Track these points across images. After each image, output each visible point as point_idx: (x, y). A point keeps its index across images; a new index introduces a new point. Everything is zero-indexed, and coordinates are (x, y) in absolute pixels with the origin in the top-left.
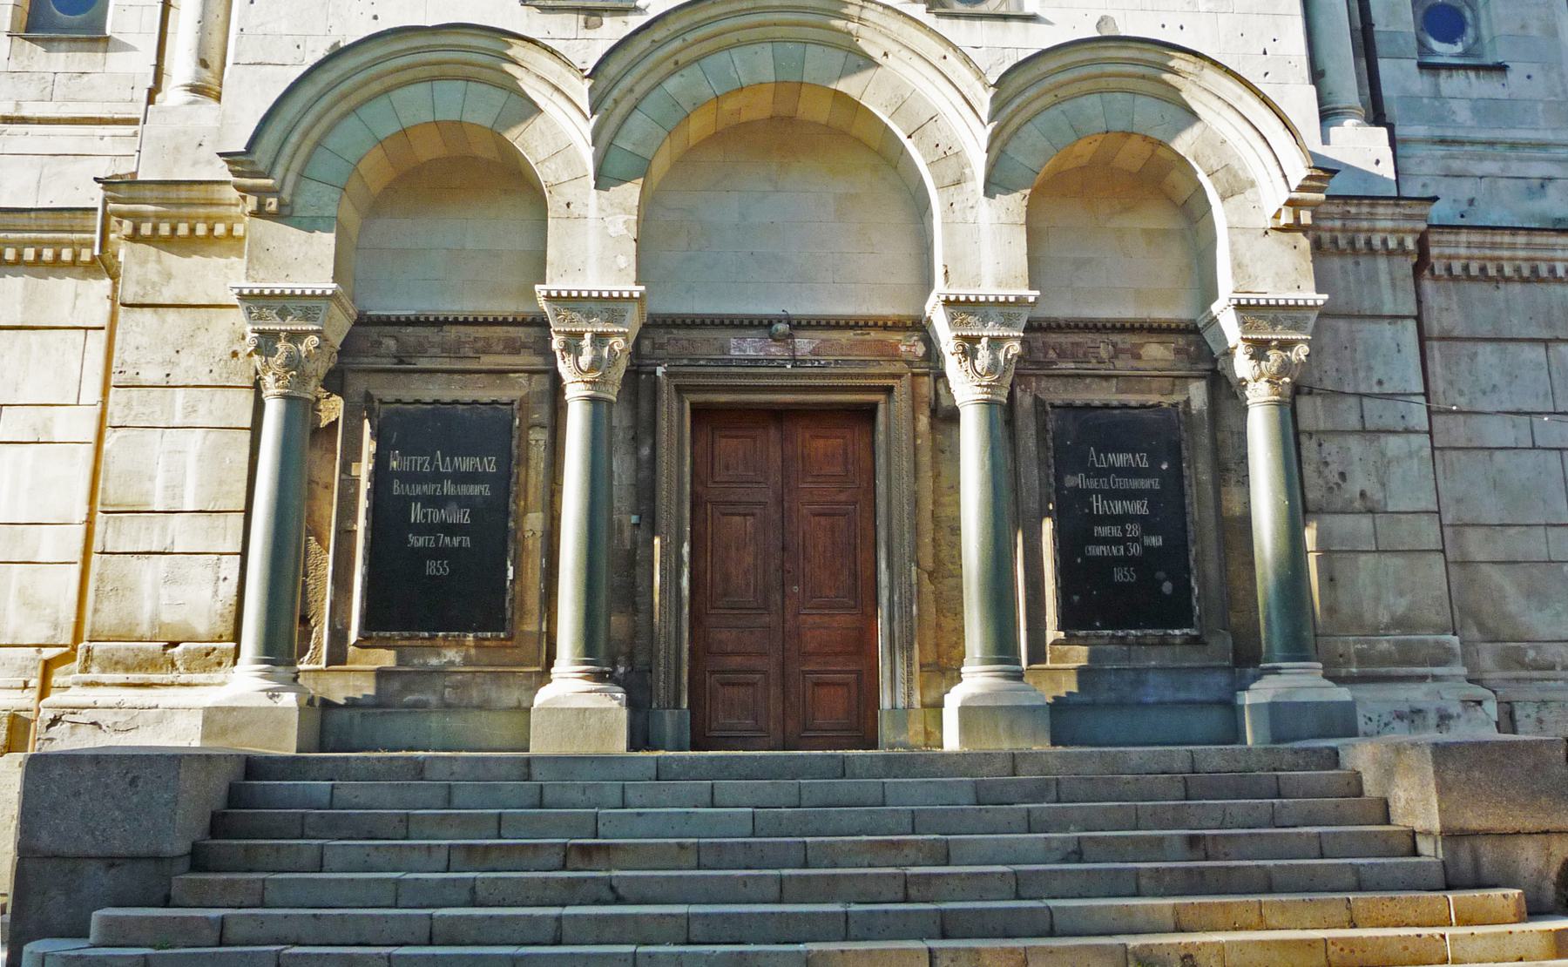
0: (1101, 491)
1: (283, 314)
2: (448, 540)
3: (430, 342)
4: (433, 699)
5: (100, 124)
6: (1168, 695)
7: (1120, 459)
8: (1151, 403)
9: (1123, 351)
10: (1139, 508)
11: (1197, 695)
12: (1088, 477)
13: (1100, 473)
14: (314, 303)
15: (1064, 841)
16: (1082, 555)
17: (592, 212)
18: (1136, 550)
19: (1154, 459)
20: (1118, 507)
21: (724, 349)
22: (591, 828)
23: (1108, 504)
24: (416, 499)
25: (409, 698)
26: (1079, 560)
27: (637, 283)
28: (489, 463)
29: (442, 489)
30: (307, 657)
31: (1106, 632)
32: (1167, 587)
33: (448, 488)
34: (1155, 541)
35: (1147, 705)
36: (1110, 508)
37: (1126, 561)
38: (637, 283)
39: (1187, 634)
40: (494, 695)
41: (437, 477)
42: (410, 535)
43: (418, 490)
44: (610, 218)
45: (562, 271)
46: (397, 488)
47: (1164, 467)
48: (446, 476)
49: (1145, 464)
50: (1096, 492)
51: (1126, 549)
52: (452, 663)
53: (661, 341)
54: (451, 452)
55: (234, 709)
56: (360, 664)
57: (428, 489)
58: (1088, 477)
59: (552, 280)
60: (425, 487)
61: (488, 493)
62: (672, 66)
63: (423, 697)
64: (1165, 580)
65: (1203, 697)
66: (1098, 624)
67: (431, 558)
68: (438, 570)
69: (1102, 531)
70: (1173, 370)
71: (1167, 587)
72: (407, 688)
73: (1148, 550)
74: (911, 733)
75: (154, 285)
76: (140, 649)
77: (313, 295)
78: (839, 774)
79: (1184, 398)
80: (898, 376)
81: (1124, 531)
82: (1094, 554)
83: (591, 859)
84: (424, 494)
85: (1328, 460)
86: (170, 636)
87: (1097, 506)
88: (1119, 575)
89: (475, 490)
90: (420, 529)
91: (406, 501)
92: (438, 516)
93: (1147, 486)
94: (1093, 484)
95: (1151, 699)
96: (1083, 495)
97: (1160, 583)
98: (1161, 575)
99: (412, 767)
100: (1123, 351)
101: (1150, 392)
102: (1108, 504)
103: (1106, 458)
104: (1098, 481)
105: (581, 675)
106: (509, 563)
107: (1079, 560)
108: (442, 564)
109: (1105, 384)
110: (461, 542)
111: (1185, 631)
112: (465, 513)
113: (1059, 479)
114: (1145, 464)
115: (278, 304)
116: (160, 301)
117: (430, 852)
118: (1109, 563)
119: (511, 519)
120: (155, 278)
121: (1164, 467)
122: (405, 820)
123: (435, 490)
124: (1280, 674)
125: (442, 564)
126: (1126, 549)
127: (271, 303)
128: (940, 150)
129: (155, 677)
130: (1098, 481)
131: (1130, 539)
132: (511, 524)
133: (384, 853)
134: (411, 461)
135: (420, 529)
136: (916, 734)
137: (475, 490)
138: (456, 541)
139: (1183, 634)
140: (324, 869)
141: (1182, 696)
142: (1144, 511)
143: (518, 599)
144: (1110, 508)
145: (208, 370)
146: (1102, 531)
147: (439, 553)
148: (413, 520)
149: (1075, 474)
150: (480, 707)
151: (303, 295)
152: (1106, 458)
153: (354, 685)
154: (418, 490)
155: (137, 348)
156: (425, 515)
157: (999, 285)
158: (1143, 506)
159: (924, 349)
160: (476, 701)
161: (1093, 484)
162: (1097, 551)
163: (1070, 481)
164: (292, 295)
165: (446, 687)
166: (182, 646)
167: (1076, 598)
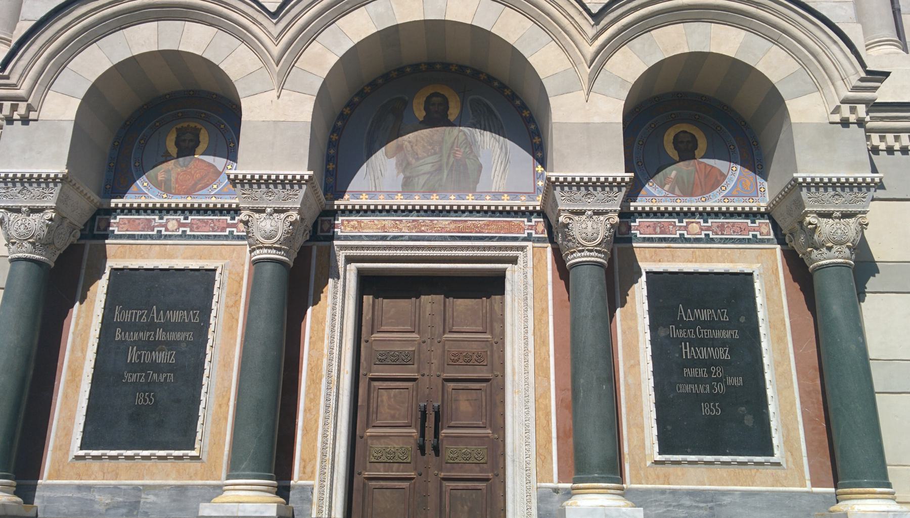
7: (705, 315)
18: (720, 389)
20: (704, 353)
33: (160, 335)
37: (712, 398)
41: (151, 326)
48: (160, 325)
49: (726, 318)
51: (712, 388)
57: (144, 336)
84: (140, 340)
87: (686, 352)
94: (682, 334)
104: (686, 332)
110: (166, 378)
118: (698, 399)
130: (686, 332)
142: (727, 357)
156: (139, 357)
161: (682, 334)
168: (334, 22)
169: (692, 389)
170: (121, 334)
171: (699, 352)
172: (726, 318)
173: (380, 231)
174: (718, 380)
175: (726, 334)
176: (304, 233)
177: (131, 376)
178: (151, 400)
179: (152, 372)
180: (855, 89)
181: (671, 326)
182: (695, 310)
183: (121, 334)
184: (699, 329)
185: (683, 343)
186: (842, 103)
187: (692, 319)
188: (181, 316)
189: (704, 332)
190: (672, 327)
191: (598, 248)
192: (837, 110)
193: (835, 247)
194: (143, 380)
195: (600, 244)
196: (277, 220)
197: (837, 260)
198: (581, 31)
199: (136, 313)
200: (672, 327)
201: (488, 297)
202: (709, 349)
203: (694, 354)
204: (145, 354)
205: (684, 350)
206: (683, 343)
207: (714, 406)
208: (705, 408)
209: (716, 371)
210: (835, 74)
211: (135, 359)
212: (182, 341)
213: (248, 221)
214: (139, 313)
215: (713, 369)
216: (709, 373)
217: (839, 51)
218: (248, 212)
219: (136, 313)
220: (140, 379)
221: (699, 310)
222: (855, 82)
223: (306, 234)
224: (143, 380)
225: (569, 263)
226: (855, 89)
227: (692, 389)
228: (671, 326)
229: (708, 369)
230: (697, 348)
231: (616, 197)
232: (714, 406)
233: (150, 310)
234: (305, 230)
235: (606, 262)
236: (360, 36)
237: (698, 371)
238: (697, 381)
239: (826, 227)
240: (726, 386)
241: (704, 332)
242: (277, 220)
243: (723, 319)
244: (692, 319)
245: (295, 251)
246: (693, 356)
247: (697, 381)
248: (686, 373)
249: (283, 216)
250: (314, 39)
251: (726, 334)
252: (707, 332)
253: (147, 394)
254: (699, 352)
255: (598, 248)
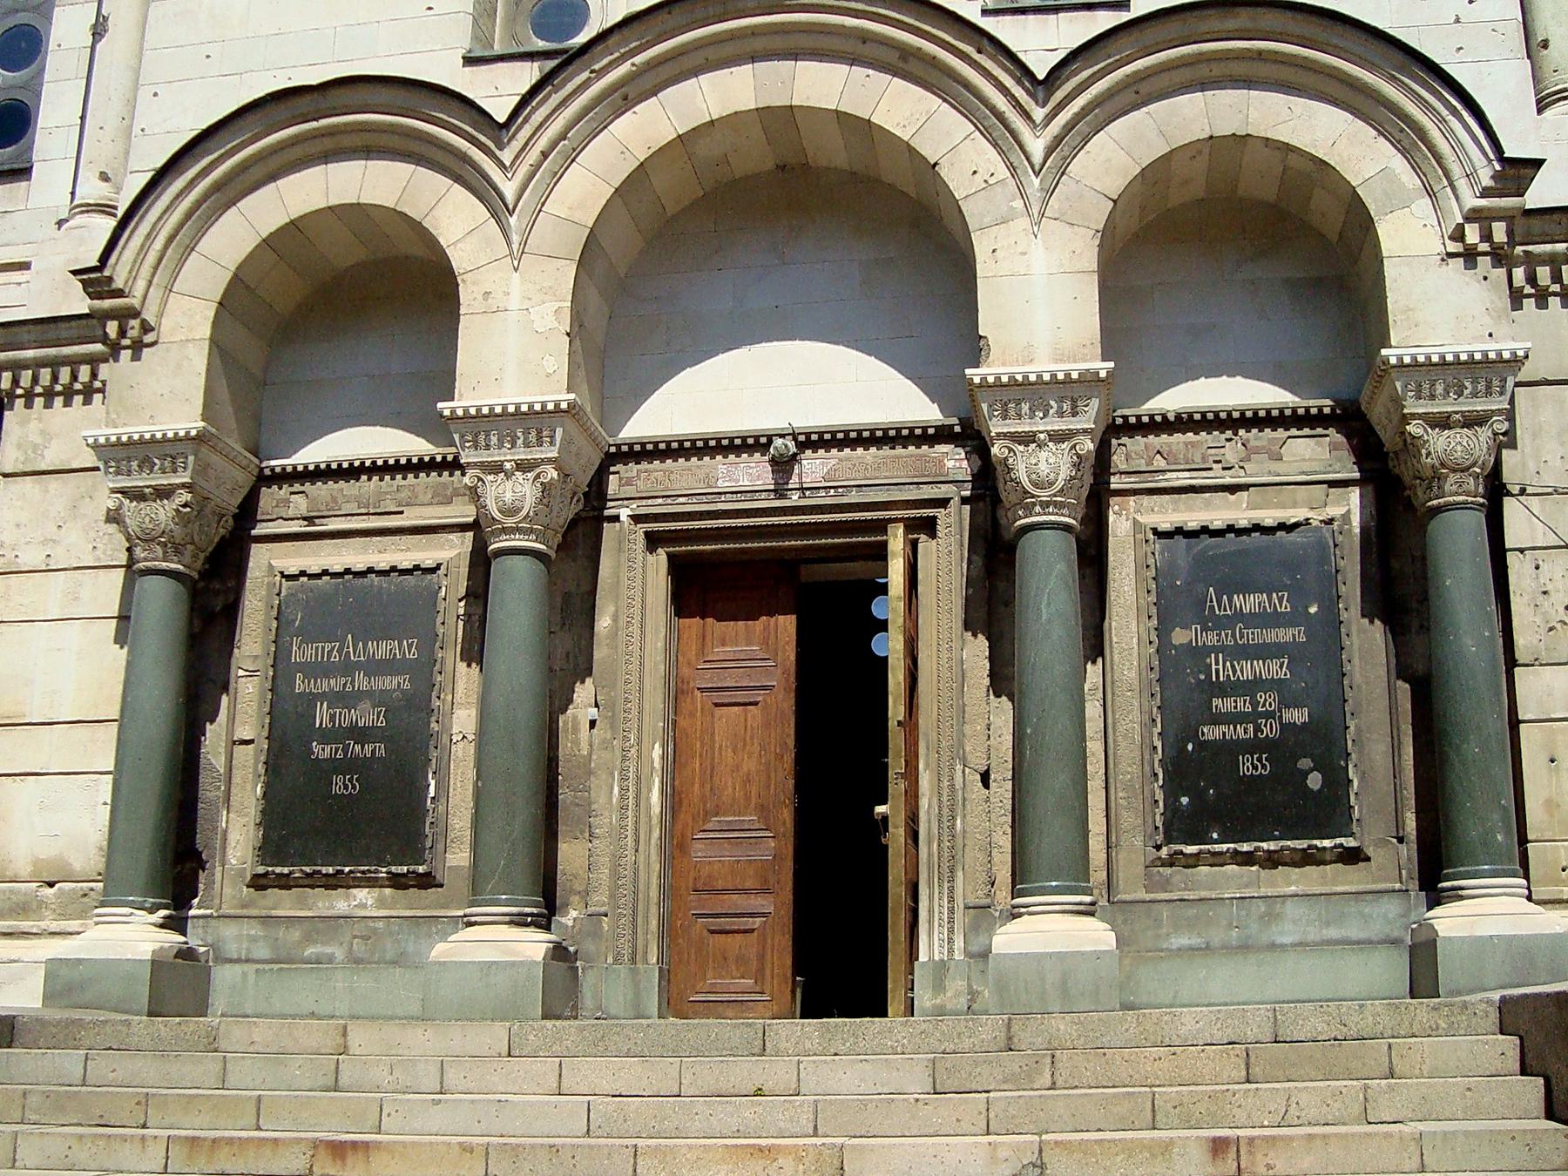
0: (1221, 649)
1: (146, 464)
2: (358, 748)
3: (344, 496)
4: (339, 953)
5: (20, 270)
6: (1313, 934)
7: (1250, 603)
8: (1293, 520)
9: (1257, 451)
10: (1276, 669)
11: (1354, 932)
12: (1205, 629)
13: (1219, 624)
14: (180, 448)
15: (1017, 1148)
16: (1194, 736)
17: (514, 303)
18: (1270, 730)
19: (1299, 596)
20: (1247, 670)
21: (709, 480)
22: (372, 1120)
23: (1233, 666)
24: (322, 696)
25: (310, 951)
26: (1190, 747)
27: (569, 390)
28: (410, 646)
29: (353, 682)
30: (196, 901)
31: (1224, 847)
32: (1315, 781)
33: (361, 681)
34: (1298, 716)
35: (1283, 947)
36: (1234, 672)
37: (1254, 746)
38: (569, 390)
39: (1341, 845)
40: (411, 948)
41: (348, 668)
42: (315, 744)
43: (324, 685)
44: (537, 308)
45: (475, 384)
46: (300, 685)
47: (1313, 610)
48: (358, 666)
49: (1285, 607)
50: (1216, 650)
51: (1257, 729)
52: (363, 906)
53: (629, 475)
54: (364, 635)
55: (79, 961)
56: (283, 909)
57: (335, 684)
58: (1205, 629)
59: (461, 395)
60: (333, 682)
61: (407, 686)
62: (620, 102)
63: (328, 950)
64: (1311, 770)
65: (1363, 935)
66: (1215, 836)
67: (337, 771)
68: (346, 788)
69: (1221, 704)
70: (1329, 473)
71: (1315, 781)
72: (308, 939)
73: (1285, 727)
74: (949, 994)
75: (35, 447)
76: (11, 891)
77: (177, 439)
78: (756, 1051)
79: (1343, 510)
80: (943, 503)
81: (1255, 704)
82: (1211, 737)
83: (343, 1158)
84: (331, 690)
85: (1549, 587)
86: (45, 874)
87: (1217, 671)
88: (1246, 766)
89: (390, 682)
90: (326, 736)
91: (312, 699)
92: (348, 717)
93: (1289, 638)
94: (1211, 639)
95: (1287, 940)
96: (1198, 653)
97: (1306, 774)
98: (1305, 763)
99: (203, 1033)
100: (1257, 451)
101: (1295, 505)
102: (1233, 666)
103: (1230, 601)
104: (1219, 635)
105: (507, 919)
106: (430, 776)
107: (1190, 747)
108: (351, 780)
109: (1232, 498)
110: (373, 751)
111: (1338, 841)
112: (379, 713)
113: (1163, 631)
114: (1285, 607)
115: (141, 452)
116: (44, 467)
117: (143, 1143)
118: (1231, 749)
119: (433, 719)
120: (39, 440)
121: (1313, 610)
122: (144, 1101)
123: (345, 685)
124: (1462, 898)
125: (351, 780)
126: (1257, 729)
127: (132, 451)
128: (979, 179)
129: (25, 925)
130: (1219, 635)
131: (1261, 716)
132: (433, 725)
133: (89, 1145)
134: (317, 648)
135: (326, 736)
136: (957, 995)
137: (390, 682)
138: (368, 748)
139: (1336, 847)
140: (17, 1164)
141: (1333, 933)
142: (1284, 674)
143: (442, 825)
144: (1234, 672)
145: (91, 547)
146: (1221, 704)
147: (347, 766)
148: (317, 726)
149: (1186, 627)
150: (394, 963)
151: (165, 440)
152: (1230, 601)
153: (248, 935)
154: (324, 685)
155: (18, 525)
156: (332, 718)
157: (1056, 361)
158: (1281, 667)
159: (980, 463)
160: (389, 956)
161: (1211, 639)
162: (1211, 733)
163: (1180, 637)
164: (153, 440)
165: (355, 937)
166: (57, 886)
167: (1185, 800)
168: (605, 127)
169: (1224, 733)
170: (303, 682)
171: (1239, 672)
172: (1286, 608)
173: (702, 485)
174: (1269, 715)
175: (1284, 635)
176: (572, 498)
177: (323, 749)
178: (354, 787)
179: (352, 742)
180: (1486, 192)
181: (1193, 627)
182: (1235, 596)
183: (303, 682)
184: (1240, 629)
185: (1213, 655)
186: (1468, 219)
187: (1229, 612)
188: (391, 650)
189: (1248, 633)
190: (1196, 629)
191: (1059, 499)
192: (1458, 235)
193: (1451, 475)
194: (340, 755)
195: (1062, 490)
196: (522, 482)
197: (1455, 498)
198: (1027, 116)
199: (323, 648)
200: (1196, 629)
201: (703, 618)
202: (1255, 662)
203: (1231, 673)
204: (340, 713)
205: (1214, 667)
206: (1213, 655)
207: (1260, 760)
208: (1244, 764)
209: (1266, 700)
210: (1456, 171)
211: (326, 722)
212: (395, 690)
213: (476, 487)
214: (327, 647)
215: (1261, 697)
216: (1255, 704)
217: (1463, 129)
218: (477, 472)
219: (323, 648)
220: (336, 754)
221: (1241, 596)
222: (1487, 181)
223: (578, 501)
224: (340, 755)
225: (1018, 523)
226: (1486, 192)
227: (1224, 733)
228: (1193, 627)
229: (1253, 697)
230: (1235, 663)
231: (1086, 406)
232: (1260, 760)
233: (343, 640)
234: (575, 494)
235: (1074, 522)
236: (886, 122)
237: (1235, 701)
238: (1234, 719)
239: (1440, 443)
240: (1281, 723)
241: (1248, 633)
242: (522, 482)
243: (1281, 607)
244: (1229, 612)
245: (557, 532)
246: (1228, 675)
247: (1234, 719)
248: (1216, 706)
249: (530, 475)
250: (573, 161)
251: (1284, 635)
252: (1253, 633)
253: (348, 777)
254: (1238, 669)
255: (1059, 499)
